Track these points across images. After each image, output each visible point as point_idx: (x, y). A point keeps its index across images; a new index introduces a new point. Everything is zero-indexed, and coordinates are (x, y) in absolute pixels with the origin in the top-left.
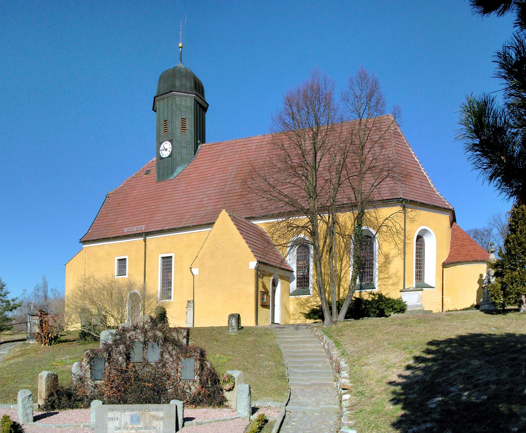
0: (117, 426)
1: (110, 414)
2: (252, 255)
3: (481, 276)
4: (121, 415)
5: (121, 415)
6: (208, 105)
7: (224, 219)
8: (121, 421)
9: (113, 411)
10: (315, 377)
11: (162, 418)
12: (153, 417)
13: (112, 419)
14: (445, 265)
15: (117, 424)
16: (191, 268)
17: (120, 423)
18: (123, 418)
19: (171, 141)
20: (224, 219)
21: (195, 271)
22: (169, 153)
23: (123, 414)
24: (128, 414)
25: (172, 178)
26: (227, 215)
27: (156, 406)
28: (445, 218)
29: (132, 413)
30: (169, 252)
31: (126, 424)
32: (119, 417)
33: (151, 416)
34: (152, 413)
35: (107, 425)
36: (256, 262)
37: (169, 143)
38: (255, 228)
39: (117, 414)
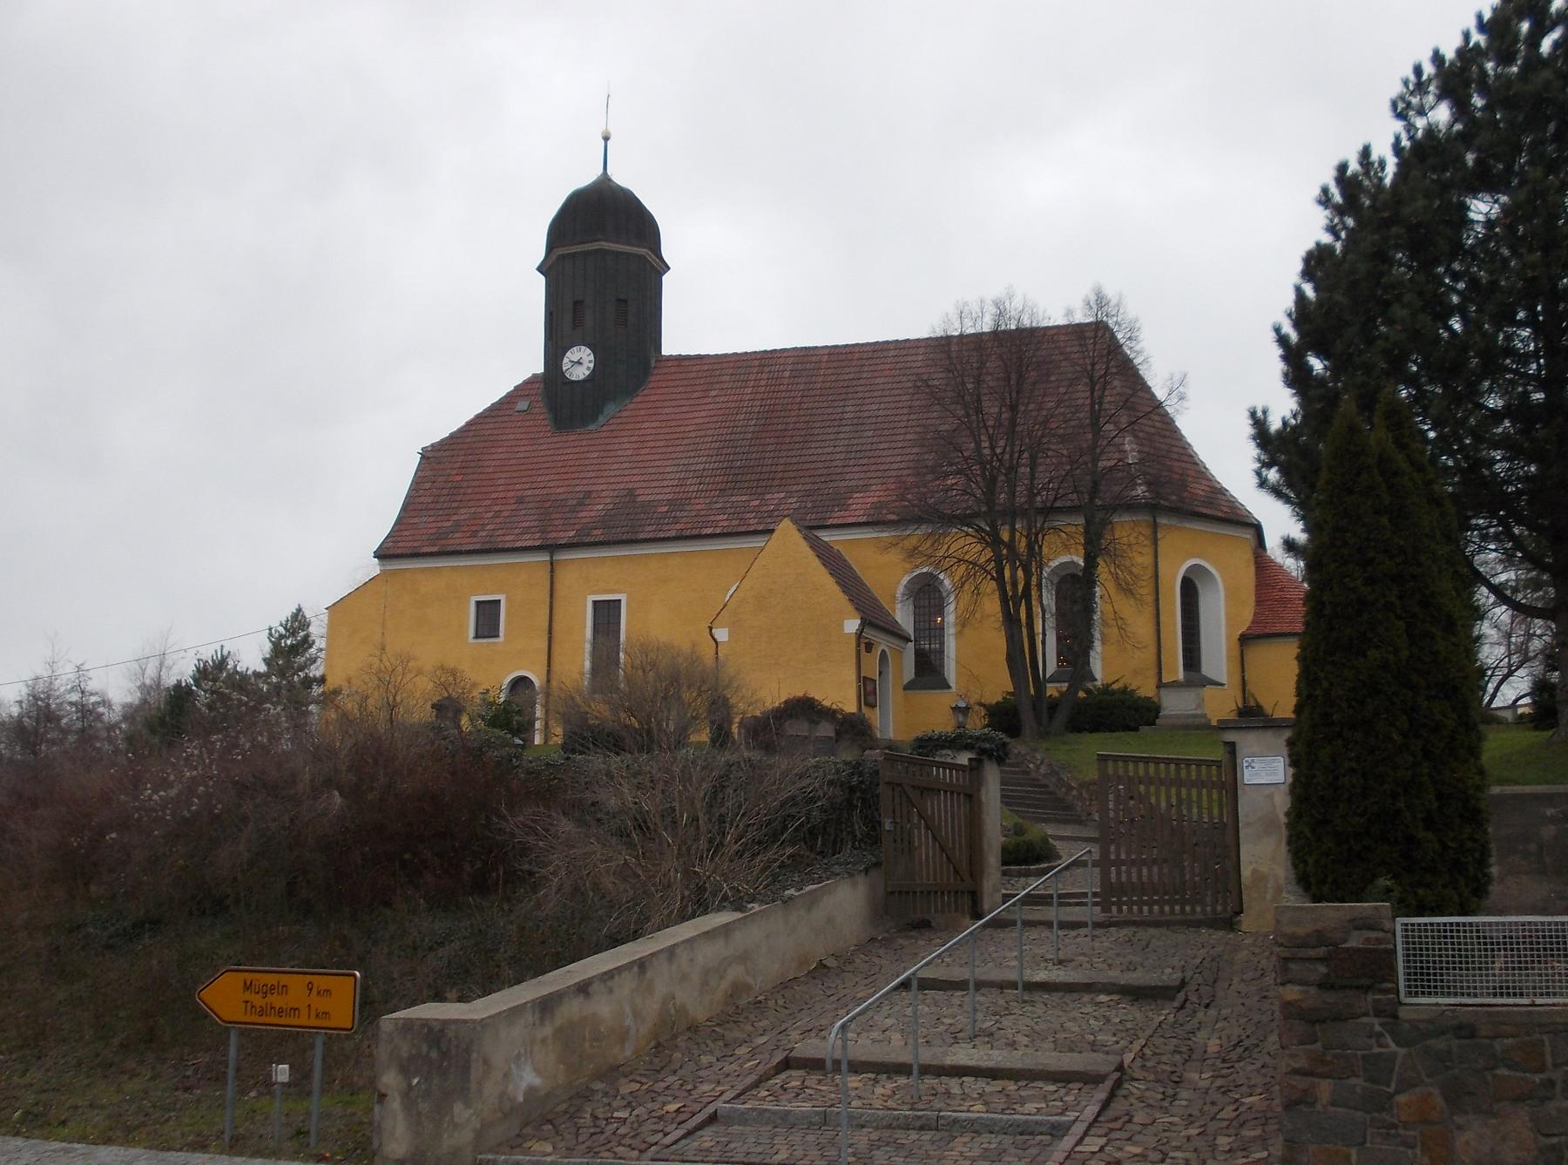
2: (850, 608)
3: (1277, 330)
14: (1245, 640)
25: (591, 427)
28: (1248, 535)
30: (613, 591)
38: (827, 546)
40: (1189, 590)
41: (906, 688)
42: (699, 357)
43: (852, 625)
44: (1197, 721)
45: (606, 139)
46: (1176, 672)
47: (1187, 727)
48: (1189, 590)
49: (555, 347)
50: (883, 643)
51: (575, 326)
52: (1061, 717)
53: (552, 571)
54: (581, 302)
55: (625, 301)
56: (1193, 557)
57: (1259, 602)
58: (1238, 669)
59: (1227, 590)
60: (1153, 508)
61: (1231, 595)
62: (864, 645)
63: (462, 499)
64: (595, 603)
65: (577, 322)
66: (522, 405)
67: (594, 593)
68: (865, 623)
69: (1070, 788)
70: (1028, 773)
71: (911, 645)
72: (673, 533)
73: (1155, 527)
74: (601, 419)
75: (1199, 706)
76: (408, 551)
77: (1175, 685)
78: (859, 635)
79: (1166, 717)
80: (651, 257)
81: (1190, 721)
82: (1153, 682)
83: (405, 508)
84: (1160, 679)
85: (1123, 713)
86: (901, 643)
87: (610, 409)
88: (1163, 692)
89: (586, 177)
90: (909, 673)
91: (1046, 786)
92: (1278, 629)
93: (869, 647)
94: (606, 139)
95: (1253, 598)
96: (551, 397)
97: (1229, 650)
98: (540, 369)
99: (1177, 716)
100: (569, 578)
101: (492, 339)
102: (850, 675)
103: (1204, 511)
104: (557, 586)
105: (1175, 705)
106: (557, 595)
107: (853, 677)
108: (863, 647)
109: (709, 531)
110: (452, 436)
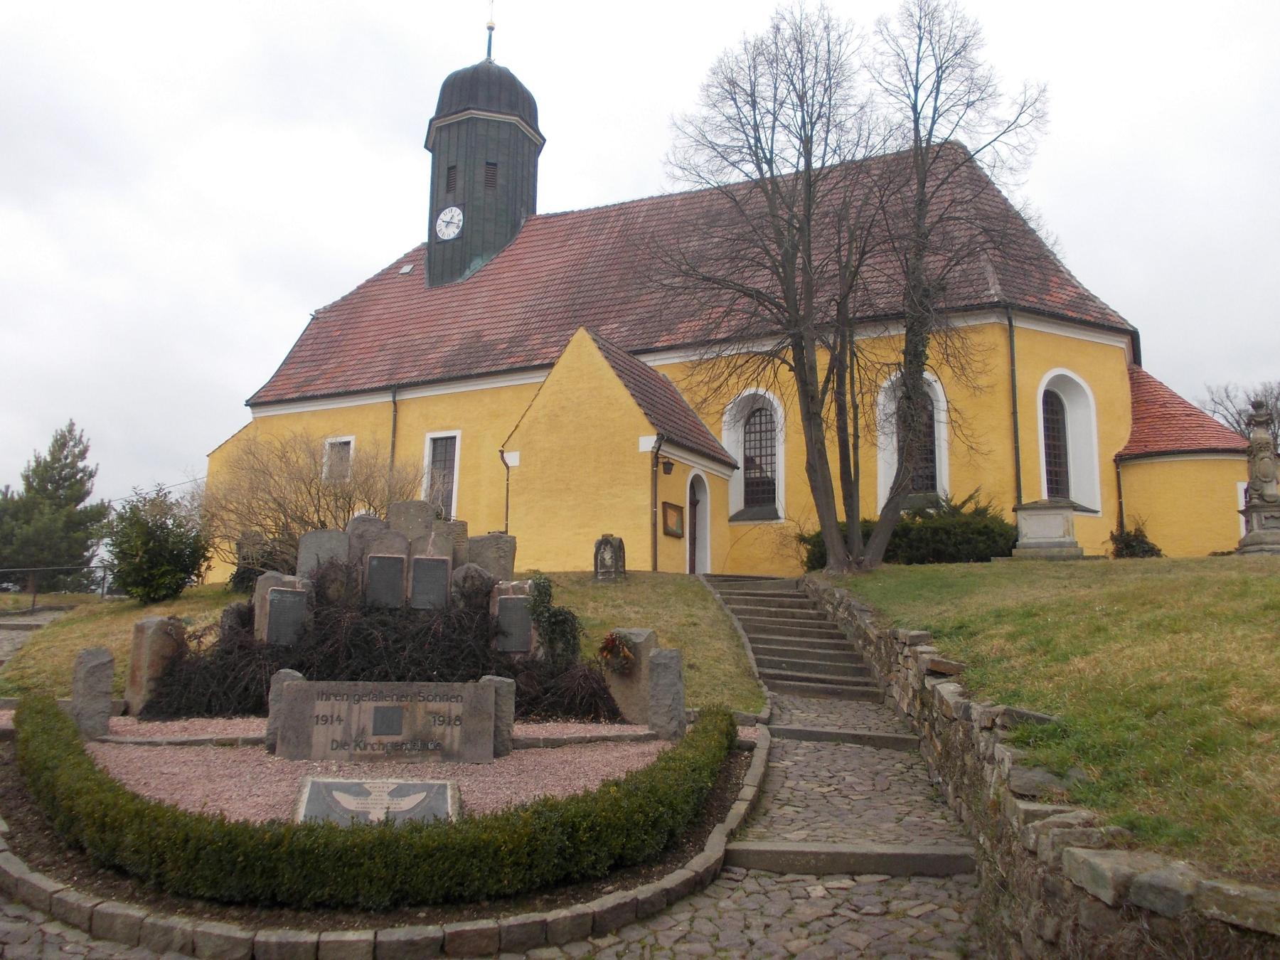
0: (339, 739)
1: (322, 707)
2: (645, 422)
4: (350, 709)
5: (350, 709)
6: (544, 140)
7: (582, 355)
8: (349, 724)
9: (328, 699)
10: (46, 883)
11: (458, 718)
12: (435, 714)
13: (326, 720)
14: (1121, 460)
15: (337, 731)
16: (502, 452)
17: (347, 731)
18: (355, 718)
19: (463, 207)
20: (582, 355)
21: (513, 458)
22: (457, 231)
23: (356, 707)
24: (369, 706)
25: (460, 281)
26: (592, 348)
27: (443, 687)
28: (1122, 343)
29: (380, 704)
30: (449, 428)
31: (362, 732)
32: (343, 715)
33: (430, 713)
34: (434, 706)
35: (309, 737)
36: (655, 438)
37: (458, 211)
38: (651, 373)
39: (341, 707)
40: (1053, 406)
41: (732, 519)
42: (565, 214)
43: (648, 442)
44: (1065, 552)
45: (491, 29)
46: (1040, 492)
47: (1051, 558)
48: (1053, 406)
49: (435, 212)
50: (690, 466)
51: (448, 191)
52: (880, 542)
53: (396, 411)
54: (454, 167)
55: (495, 165)
56: (1058, 365)
57: (1136, 420)
58: (1115, 494)
59: (1098, 404)
60: (1007, 309)
61: (1104, 411)
62: (662, 466)
63: (339, 353)
64: (435, 441)
65: (450, 187)
66: (406, 269)
67: (431, 430)
68: (662, 439)
69: (868, 641)
70: (824, 617)
71: (738, 477)
72: (504, 367)
73: (1010, 331)
74: (468, 273)
75: (1068, 532)
76: (274, 399)
77: (1036, 507)
78: (656, 456)
79: (1026, 547)
80: (524, 127)
81: (1056, 551)
82: (1009, 504)
83: (284, 363)
84: (1019, 497)
85: (978, 540)
86: (726, 471)
87: (477, 264)
88: (1021, 514)
89: (471, 57)
90: (736, 501)
91: (843, 637)
92: (1163, 446)
93: (668, 467)
94: (491, 29)
95: (1129, 417)
96: (439, 262)
97: (1102, 472)
98: (426, 240)
99: (1039, 546)
100: (409, 417)
101: (387, 212)
102: (643, 498)
103: (1070, 314)
104: (400, 425)
105: (1037, 530)
106: (401, 432)
107: (647, 501)
108: (661, 467)
109: (536, 363)
110: (344, 299)
